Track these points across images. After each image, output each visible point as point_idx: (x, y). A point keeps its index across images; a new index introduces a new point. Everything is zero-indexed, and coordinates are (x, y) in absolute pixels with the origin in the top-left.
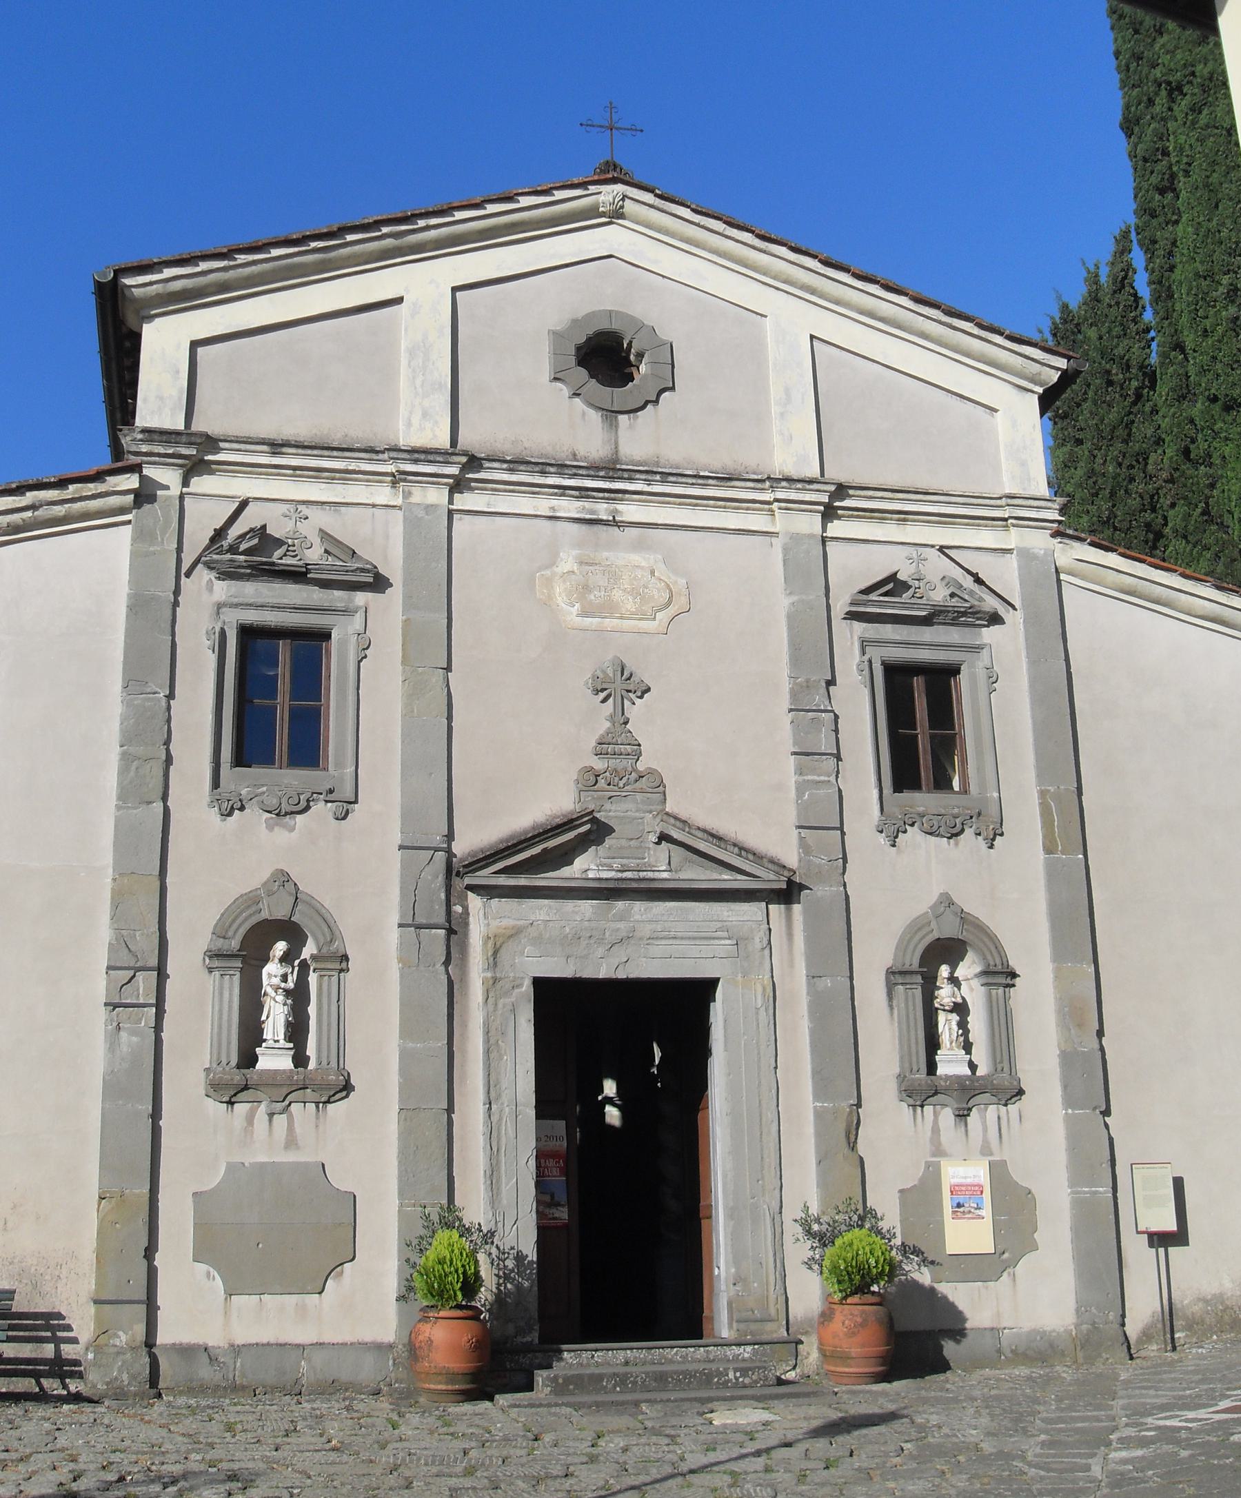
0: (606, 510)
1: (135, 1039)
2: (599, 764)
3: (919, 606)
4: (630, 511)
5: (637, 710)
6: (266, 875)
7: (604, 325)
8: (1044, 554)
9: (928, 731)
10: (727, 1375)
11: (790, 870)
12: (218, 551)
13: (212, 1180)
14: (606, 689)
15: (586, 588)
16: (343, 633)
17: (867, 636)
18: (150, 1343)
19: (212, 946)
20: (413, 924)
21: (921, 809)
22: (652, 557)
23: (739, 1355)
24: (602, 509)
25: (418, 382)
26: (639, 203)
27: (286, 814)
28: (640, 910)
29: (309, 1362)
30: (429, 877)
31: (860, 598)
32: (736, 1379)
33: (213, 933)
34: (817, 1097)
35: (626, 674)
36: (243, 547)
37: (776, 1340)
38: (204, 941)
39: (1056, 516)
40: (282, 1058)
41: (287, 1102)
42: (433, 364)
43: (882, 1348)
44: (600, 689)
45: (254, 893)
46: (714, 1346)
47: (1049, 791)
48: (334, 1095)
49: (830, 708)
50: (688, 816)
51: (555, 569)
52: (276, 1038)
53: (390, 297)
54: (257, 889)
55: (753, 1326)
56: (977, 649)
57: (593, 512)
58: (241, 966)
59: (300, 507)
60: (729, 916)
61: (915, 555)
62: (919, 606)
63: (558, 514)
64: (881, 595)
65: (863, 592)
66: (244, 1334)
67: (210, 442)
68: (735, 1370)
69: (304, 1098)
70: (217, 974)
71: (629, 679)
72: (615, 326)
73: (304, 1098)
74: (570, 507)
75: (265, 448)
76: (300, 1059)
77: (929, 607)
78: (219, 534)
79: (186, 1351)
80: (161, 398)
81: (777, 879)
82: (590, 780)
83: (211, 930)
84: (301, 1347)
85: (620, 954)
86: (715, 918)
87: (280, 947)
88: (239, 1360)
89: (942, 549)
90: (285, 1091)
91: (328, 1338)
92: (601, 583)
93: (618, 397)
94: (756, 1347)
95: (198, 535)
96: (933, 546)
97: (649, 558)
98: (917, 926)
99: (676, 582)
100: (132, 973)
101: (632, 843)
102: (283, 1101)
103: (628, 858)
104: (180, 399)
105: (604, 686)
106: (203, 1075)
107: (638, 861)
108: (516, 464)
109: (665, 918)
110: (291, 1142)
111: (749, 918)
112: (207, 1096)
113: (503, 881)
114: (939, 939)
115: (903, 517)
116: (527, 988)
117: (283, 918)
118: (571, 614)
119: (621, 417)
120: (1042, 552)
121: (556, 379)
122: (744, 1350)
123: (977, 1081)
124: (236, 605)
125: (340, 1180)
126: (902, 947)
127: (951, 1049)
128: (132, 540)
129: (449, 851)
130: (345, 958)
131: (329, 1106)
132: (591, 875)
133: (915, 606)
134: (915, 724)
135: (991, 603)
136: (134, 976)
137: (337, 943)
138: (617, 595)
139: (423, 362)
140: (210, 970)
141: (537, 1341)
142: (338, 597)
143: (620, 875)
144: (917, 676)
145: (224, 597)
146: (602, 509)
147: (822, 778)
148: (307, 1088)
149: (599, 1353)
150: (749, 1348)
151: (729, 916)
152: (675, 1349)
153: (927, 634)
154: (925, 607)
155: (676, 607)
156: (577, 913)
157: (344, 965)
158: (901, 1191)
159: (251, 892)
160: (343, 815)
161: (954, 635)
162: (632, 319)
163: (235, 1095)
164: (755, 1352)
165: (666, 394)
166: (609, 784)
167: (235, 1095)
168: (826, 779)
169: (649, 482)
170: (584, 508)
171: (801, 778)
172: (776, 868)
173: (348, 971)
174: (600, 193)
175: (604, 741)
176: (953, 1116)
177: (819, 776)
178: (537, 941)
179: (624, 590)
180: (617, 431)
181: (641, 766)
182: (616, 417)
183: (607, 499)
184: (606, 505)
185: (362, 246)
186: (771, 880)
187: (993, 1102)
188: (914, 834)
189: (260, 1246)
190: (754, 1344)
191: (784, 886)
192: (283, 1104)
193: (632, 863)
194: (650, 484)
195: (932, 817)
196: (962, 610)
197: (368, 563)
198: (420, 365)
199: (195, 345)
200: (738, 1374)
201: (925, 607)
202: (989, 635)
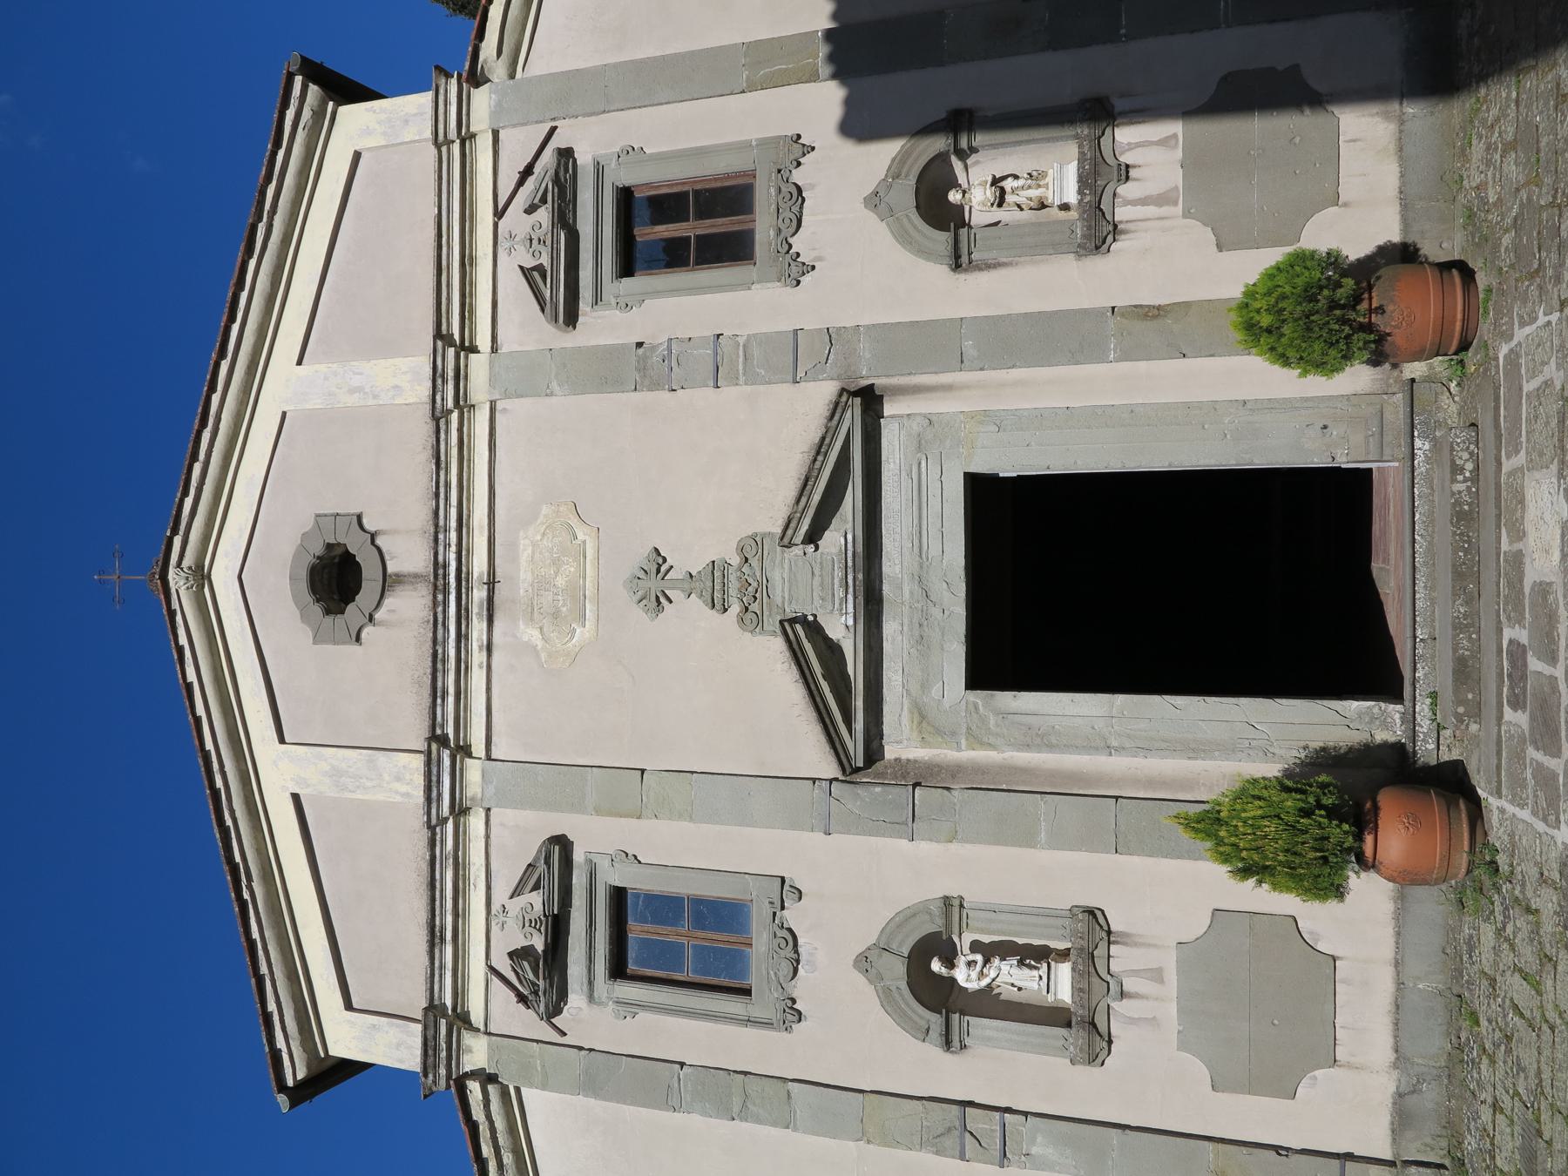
0: (478, 589)
1: (1039, 1139)
2: (735, 609)
3: (555, 242)
4: (479, 565)
5: (688, 559)
6: (861, 979)
7: (304, 586)
8: (495, 93)
9: (691, 223)
10: (1460, 492)
11: (840, 395)
12: (536, 1005)
13: (1199, 1071)
14: (657, 598)
15: (556, 615)
16: (612, 876)
17: (591, 301)
18: (1391, 1164)
19: (938, 1043)
20: (909, 824)
21: (772, 233)
22: (522, 542)
23: (1426, 456)
24: (479, 594)
25: (369, 784)
26: (183, 551)
27: (796, 952)
28: (894, 564)
29: (1419, 978)
30: (859, 803)
31: (549, 311)
32: (1465, 481)
33: (924, 1040)
34: (1102, 359)
35: (642, 575)
36: (531, 976)
37: (1409, 421)
38: (932, 1051)
39: (454, 82)
40: (1059, 974)
41: (1108, 978)
42: (350, 767)
43: (1428, 270)
44: (659, 602)
45: (880, 992)
46: (1413, 487)
47: (748, 77)
48: (1101, 927)
49: (666, 344)
50: (786, 508)
51: (539, 647)
52: (1038, 979)
53: (292, 807)
54: (877, 991)
55: (1388, 438)
56: (599, 170)
57: (481, 607)
58: (957, 1015)
59: (494, 911)
60: (894, 462)
61: (507, 245)
62: (555, 242)
63: (485, 643)
64: (545, 284)
65: (543, 310)
66: (1380, 1047)
67: (433, 1009)
68: (1454, 481)
69: (1103, 957)
70: (968, 1041)
71: (646, 572)
72: (303, 574)
73: (1103, 957)
74: (478, 629)
75: (437, 951)
76: (1064, 955)
77: (555, 230)
78: (522, 998)
79: (1402, 1119)
80: (398, 1045)
81: (850, 408)
82: (751, 619)
83: (919, 1043)
84: (1400, 985)
85: (938, 589)
86: (896, 478)
87: (936, 966)
88: (1416, 1060)
89: (499, 214)
90: (1095, 979)
91: (1387, 950)
92: (550, 598)
93: (370, 572)
94: (1416, 434)
95: (525, 1022)
96: (496, 226)
97: (524, 545)
98: (904, 238)
99: (545, 516)
100: (967, 1135)
101: (817, 572)
102: (1108, 983)
103: (833, 578)
104: (398, 1026)
105: (653, 599)
106: (1079, 1068)
107: (836, 568)
108: (436, 694)
109: (898, 537)
110: (1157, 975)
111: (896, 439)
112: (1102, 1064)
113: (859, 725)
114: (916, 207)
115: (467, 261)
116: (978, 696)
117: (906, 966)
118: (583, 633)
119: (390, 570)
120: (493, 96)
121: (358, 639)
122: (1420, 449)
123: (1085, 155)
124: (591, 983)
125: (1198, 924)
126: (924, 253)
127: (1047, 186)
128: (531, 1087)
129: (831, 781)
130: (947, 900)
131: (1113, 928)
132: (850, 622)
133: (555, 246)
134: (687, 237)
135: (548, 157)
136: (969, 1132)
137: (932, 907)
138: (560, 581)
139: (350, 777)
140: (963, 1047)
141: (1399, 707)
142: (579, 881)
143: (851, 590)
144: (634, 237)
145: (582, 997)
146: (479, 594)
147: (741, 353)
148: (1092, 954)
149: (1419, 632)
150: (1418, 443)
151: (894, 462)
152: (1416, 537)
153: (585, 227)
154: (555, 234)
155: (571, 516)
156: (894, 640)
157: (956, 903)
158: (1220, 248)
159: (879, 996)
160: (796, 892)
161: (585, 197)
162: (296, 556)
163: (1101, 1036)
164: (1424, 436)
165: (365, 521)
166: (755, 598)
167: (1101, 1036)
168: (741, 348)
169: (447, 546)
170: (478, 614)
171: (742, 379)
172: (839, 410)
173: (962, 897)
174: (177, 591)
175: (710, 600)
176: (1128, 184)
177: (738, 356)
178: (925, 686)
179: (556, 574)
180: (402, 575)
181: (735, 560)
182: (390, 576)
183: (467, 589)
184: (475, 591)
185: (243, 837)
186: (853, 417)
187: (1111, 132)
188: (798, 243)
189: (1276, 1022)
190: (1413, 436)
191: (858, 401)
192: (1111, 982)
193: (839, 574)
194: (449, 544)
195: (780, 219)
196: (556, 190)
197: (539, 851)
198: (353, 780)
199: (349, 1006)
200: (1460, 478)
201: (555, 234)
202: (584, 158)
